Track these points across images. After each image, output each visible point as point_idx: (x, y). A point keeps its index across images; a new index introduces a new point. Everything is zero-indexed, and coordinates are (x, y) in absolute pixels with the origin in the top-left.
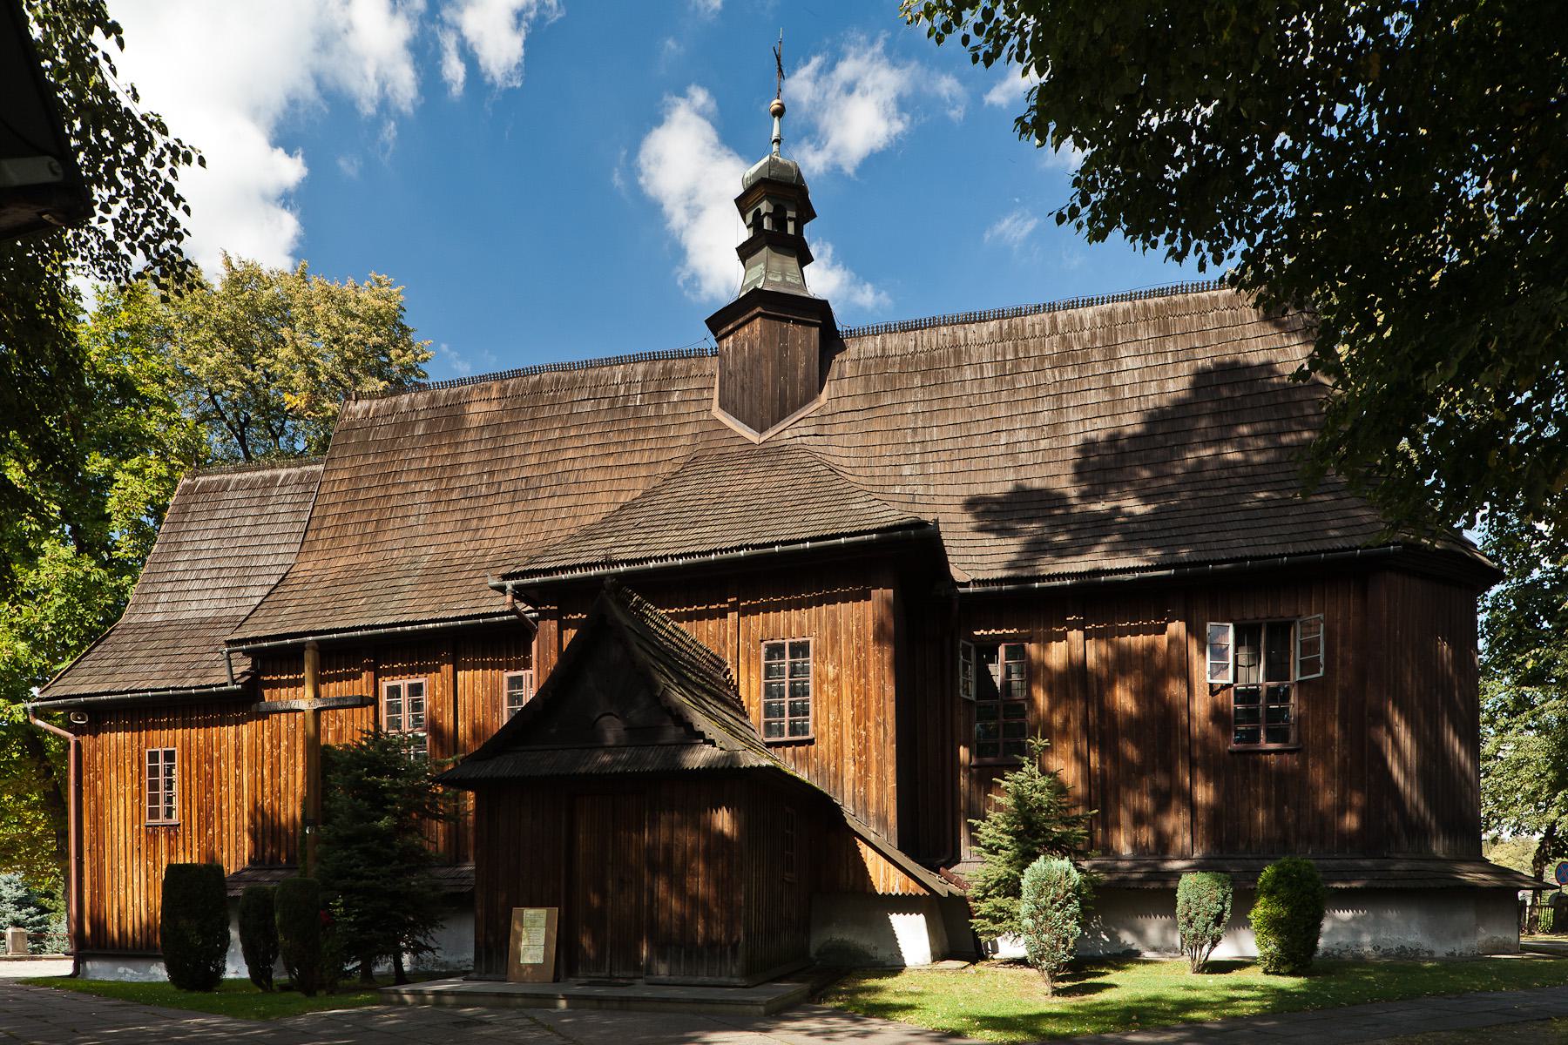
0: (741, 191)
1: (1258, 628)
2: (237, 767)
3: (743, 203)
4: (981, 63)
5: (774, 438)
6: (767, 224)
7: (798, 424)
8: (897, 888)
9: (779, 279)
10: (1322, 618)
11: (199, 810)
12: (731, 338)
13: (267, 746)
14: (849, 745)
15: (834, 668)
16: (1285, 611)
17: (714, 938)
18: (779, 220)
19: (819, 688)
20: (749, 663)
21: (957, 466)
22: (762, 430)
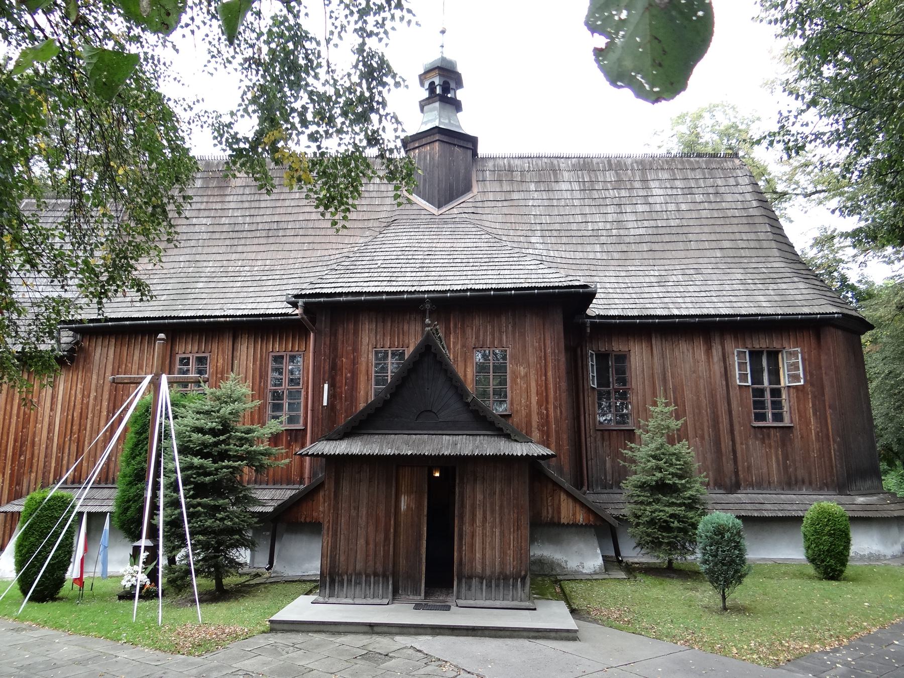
0: (422, 72)
1: (761, 352)
2: (52, 410)
3: (422, 78)
4: (787, 93)
5: (447, 212)
6: (438, 90)
7: (462, 205)
8: (581, 520)
9: (447, 121)
10: (799, 350)
11: (15, 441)
12: (417, 151)
13: (79, 396)
14: (535, 419)
15: (524, 368)
16: (776, 345)
17: (508, 573)
18: (446, 88)
19: (514, 381)
20: (465, 362)
21: (564, 240)
22: (439, 207)
